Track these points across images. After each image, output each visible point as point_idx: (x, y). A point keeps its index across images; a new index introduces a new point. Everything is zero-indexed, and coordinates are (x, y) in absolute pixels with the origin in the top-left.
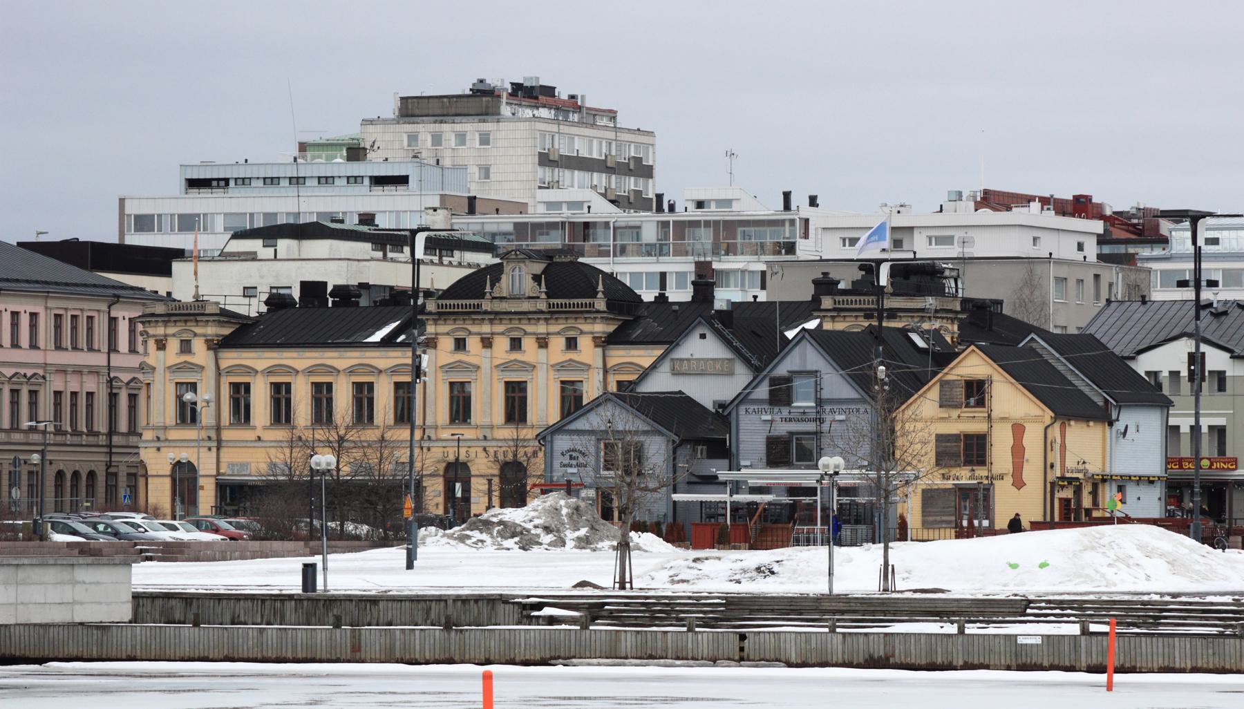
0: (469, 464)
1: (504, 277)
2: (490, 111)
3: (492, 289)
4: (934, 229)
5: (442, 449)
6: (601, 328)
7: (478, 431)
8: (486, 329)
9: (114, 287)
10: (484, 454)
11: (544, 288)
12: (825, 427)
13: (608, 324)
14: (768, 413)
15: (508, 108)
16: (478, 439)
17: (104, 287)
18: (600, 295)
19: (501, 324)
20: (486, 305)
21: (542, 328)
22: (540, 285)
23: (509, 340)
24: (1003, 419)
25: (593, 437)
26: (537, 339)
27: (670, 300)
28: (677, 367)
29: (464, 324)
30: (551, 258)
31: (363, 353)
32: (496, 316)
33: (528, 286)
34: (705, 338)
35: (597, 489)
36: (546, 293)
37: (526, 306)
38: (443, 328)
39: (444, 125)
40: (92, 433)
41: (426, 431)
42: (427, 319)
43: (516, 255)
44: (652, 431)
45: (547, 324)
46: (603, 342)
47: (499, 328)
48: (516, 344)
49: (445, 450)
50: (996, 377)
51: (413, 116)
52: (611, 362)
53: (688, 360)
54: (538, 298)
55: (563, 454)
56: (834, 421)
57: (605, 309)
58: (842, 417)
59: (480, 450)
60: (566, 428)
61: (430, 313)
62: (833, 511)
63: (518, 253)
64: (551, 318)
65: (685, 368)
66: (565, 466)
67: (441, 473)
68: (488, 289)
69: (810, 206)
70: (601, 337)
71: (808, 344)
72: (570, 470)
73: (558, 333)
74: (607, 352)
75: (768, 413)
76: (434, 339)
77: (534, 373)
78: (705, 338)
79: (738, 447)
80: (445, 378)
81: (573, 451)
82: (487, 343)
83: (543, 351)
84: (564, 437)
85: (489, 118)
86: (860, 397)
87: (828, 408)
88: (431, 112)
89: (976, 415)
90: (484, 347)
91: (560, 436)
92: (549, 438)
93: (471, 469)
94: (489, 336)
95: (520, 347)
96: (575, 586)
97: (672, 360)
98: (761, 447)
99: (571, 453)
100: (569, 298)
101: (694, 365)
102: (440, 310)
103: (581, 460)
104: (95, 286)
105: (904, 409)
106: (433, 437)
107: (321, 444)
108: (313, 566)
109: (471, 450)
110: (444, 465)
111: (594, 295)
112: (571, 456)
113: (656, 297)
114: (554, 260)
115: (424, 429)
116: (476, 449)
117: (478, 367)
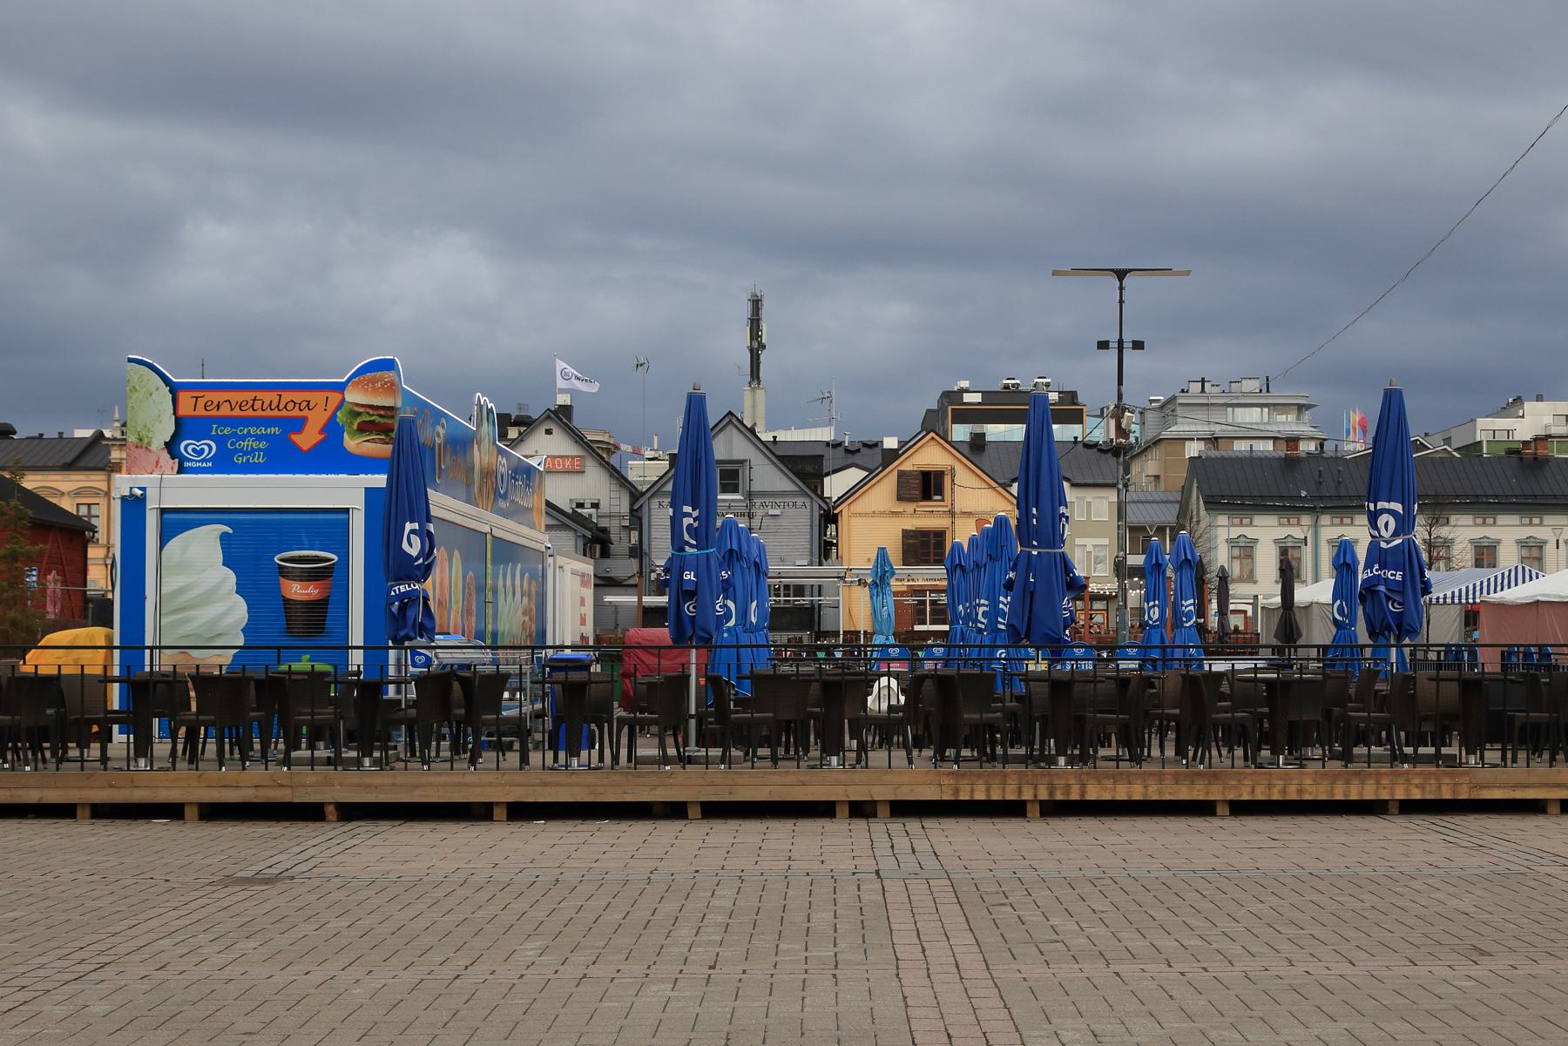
4: (112, 525)
12: (756, 523)
14: (770, 507)
24: (969, 514)
40: (1460, 603)
50: (959, 468)
56: (767, 515)
58: (777, 512)
62: (1256, 670)
69: (1098, 342)
71: (735, 431)
75: (770, 507)
78: (551, 433)
79: (649, 545)
86: (797, 489)
87: (758, 501)
89: (935, 509)
96: (114, 554)
98: (1469, 557)
105: (850, 503)
107: (631, 582)
115: (109, 548)
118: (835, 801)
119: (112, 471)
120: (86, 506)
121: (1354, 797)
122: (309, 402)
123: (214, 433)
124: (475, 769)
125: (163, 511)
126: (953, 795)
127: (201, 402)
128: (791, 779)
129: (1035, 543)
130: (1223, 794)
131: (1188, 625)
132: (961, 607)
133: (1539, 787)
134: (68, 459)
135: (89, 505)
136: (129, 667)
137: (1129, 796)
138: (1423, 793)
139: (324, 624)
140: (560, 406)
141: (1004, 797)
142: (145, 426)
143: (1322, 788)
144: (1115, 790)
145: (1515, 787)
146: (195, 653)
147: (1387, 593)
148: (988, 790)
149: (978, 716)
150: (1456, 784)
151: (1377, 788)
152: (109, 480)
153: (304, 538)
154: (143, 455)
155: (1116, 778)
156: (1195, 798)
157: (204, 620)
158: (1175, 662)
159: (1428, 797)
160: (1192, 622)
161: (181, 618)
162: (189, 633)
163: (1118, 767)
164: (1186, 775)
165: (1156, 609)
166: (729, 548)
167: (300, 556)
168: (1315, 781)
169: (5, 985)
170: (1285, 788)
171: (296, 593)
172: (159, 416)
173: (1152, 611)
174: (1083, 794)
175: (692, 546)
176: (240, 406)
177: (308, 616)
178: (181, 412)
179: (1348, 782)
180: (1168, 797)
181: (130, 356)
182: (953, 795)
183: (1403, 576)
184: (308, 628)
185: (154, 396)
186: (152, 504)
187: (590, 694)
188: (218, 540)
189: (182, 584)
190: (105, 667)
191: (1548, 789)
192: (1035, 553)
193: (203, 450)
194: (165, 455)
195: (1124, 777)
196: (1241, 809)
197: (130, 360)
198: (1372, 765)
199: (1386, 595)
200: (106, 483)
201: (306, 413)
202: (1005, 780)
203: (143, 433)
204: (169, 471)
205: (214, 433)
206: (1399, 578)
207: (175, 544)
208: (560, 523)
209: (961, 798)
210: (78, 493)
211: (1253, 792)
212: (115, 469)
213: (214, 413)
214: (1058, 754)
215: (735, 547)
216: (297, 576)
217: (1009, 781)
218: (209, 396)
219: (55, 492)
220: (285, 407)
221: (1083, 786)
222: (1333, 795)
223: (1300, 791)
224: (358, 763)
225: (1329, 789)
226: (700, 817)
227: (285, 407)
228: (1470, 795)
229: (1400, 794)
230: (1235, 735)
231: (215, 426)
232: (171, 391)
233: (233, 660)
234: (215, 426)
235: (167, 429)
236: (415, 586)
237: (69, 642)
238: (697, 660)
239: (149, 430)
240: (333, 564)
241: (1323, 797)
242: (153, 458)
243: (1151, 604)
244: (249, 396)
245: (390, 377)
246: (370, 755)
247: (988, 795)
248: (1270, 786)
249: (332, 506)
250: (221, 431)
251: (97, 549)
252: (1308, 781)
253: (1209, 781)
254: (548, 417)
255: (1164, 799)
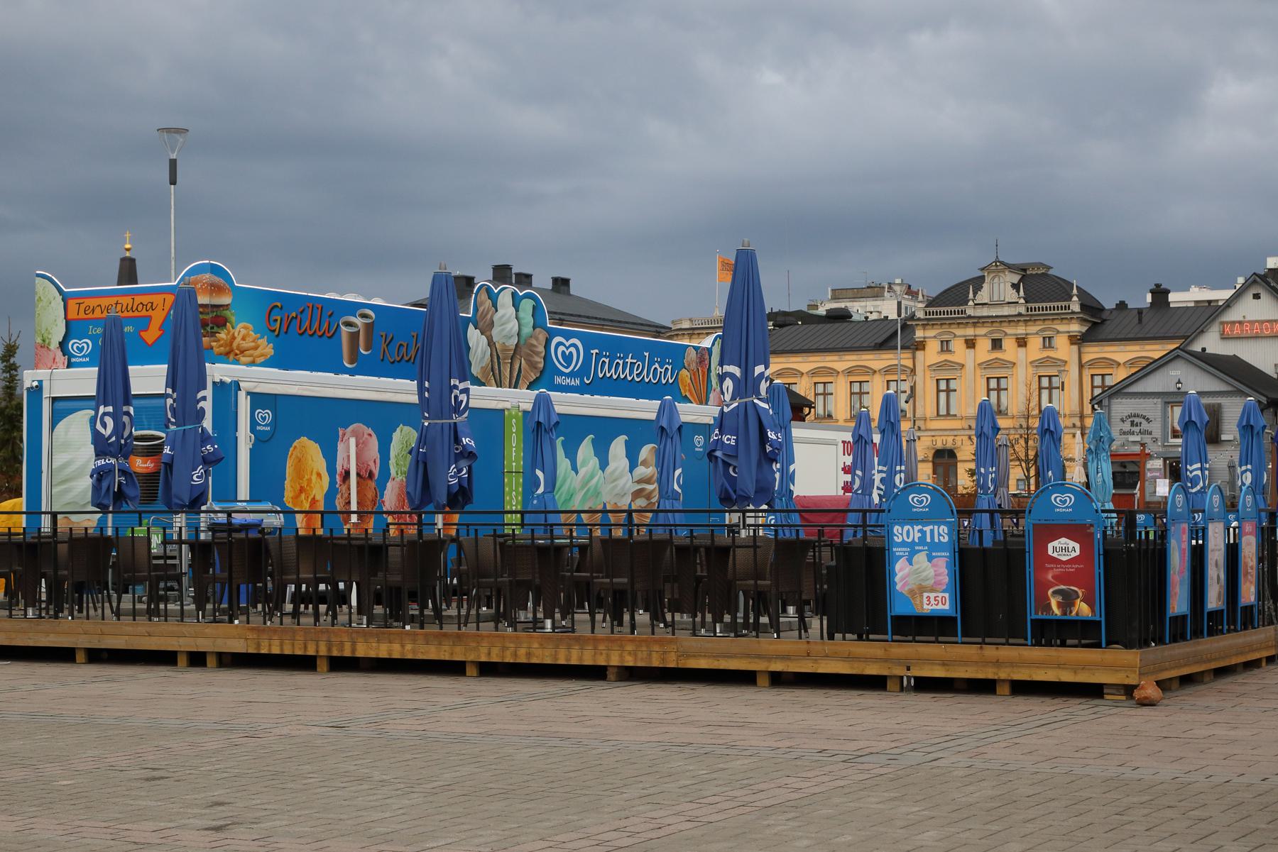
0: (955, 451)
1: (985, 286)
2: (880, 295)
3: (974, 297)
5: (930, 438)
6: (1076, 328)
7: (963, 421)
8: (970, 332)
9: (657, 327)
10: (970, 442)
11: (1022, 293)
13: (1082, 325)
15: (888, 294)
16: (963, 429)
17: (649, 326)
18: (1075, 298)
19: (983, 327)
20: (970, 312)
21: (1021, 330)
22: (1018, 291)
23: (990, 341)
25: (1159, 400)
26: (1017, 339)
27: (1129, 307)
28: (1227, 329)
29: (950, 328)
30: (1025, 270)
31: (859, 356)
32: (977, 321)
33: (1011, 295)
34: (1259, 298)
35: (1165, 460)
36: (1024, 299)
37: (1006, 311)
38: (931, 333)
39: (855, 303)
41: (916, 422)
42: (917, 325)
43: (996, 266)
44: (1235, 391)
45: (1026, 326)
46: (1079, 340)
47: (981, 331)
48: (997, 344)
49: (934, 439)
51: (839, 299)
52: (1086, 358)
53: (1240, 322)
54: (1017, 303)
55: (1123, 421)
57: (1079, 310)
59: (966, 438)
60: (1126, 391)
61: (919, 319)
63: (998, 264)
64: (1030, 320)
65: (1237, 331)
66: (1124, 433)
67: (931, 459)
68: (971, 296)
70: (1077, 336)
72: (1132, 438)
73: (1037, 333)
74: (1082, 349)
76: (923, 342)
77: (1014, 369)
78: (1259, 298)
80: (933, 376)
81: (1135, 416)
82: (970, 344)
83: (1022, 350)
84: (1124, 400)
85: (879, 298)
88: (848, 297)
90: (968, 347)
91: (1119, 400)
92: (1105, 402)
93: (958, 455)
94: (973, 338)
95: (1001, 347)
97: (1223, 323)
99: (1132, 419)
100: (1051, 301)
101: (1247, 327)
102: (928, 317)
103: (1145, 426)
104: (642, 325)
106: (923, 428)
108: (1035, 614)
109: (957, 438)
110: (933, 451)
111: (1070, 298)
112: (1132, 423)
113: (1117, 305)
114: (1028, 272)
115: (914, 421)
116: (962, 437)
117: (963, 366)
118: (755, 671)
119: (917, 349)
120: (1047, 378)
121: (574, 661)
122: (152, 303)
123: (90, 333)
124: (73, 619)
125: (54, 399)
126: (255, 649)
127: (82, 307)
128: (141, 629)
129: (426, 415)
130: (465, 655)
131: (1194, 490)
132: (1050, 473)
133: (741, 658)
134: (880, 340)
135: (1103, 376)
136: (117, 528)
137: (389, 654)
138: (635, 660)
139: (141, 493)
140: (1270, 270)
141: (293, 652)
142: (47, 330)
143: (547, 652)
144: (378, 648)
145: (716, 657)
146: (74, 518)
147: (726, 459)
148: (281, 645)
149: (614, 580)
150: (665, 652)
151: (595, 654)
152: (914, 358)
153: (144, 420)
154: (46, 353)
155: (459, 638)
156: (442, 658)
157: (79, 490)
158: (859, 528)
159: (639, 664)
160: (1198, 487)
161: (65, 488)
162: (69, 501)
163: (478, 629)
164: (436, 636)
165: (1249, 474)
166: (536, 420)
167: (141, 435)
168: (541, 645)
169: (631, 834)
170: (516, 652)
171: (139, 467)
172: (55, 320)
173: (1244, 476)
174: (354, 650)
175: (173, 424)
176: (108, 310)
177: (147, 486)
178: (70, 317)
179: (569, 648)
180: (420, 657)
181: (38, 272)
182: (255, 649)
183: (737, 441)
184: (148, 497)
185: (52, 304)
186: (46, 394)
187: (591, 556)
188: (88, 423)
189: (65, 460)
190: (102, 528)
191: (750, 660)
192: (426, 424)
193: (83, 347)
194: (59, 353)
195: (386, 636)
196: (489, 670)
197: (38, 275)
198: (121, 618)
199: (723, 461)
200: (912, 360)
201: (150, 312)
202: (294, 637)
203: (45, 335)
204: (61, 366)
205: (90, 333)
206: (733, 442)
207: (61, 426)
208: (1235, 389)
209: (263, 652)
210: (813, 373)
211: (489, 654)
212: (919, 347)
213: (90, 316)
214: (546, 617)
215: (541, 420)
216: (140, 453)
217: (297, 638)
218: (88, 302)
219: (1111, 362)
220: (137, 309)
221: (354, 644)
222: (556, 659)
223: (529, 655)
224: (536, 624)
225: (553, 653)
226: (84, 661)
227: (137, 309)
228: (678, 663)
229: (615, 661)
230: (587, 595)
231: (91, 327)
232: (63, 300)
233: (98, 524)
234: (91, 327)
235: (58, 332)
236: (109, 460)
237: (10, 508)
238: (113, 523)
239: (49, 333)
240: (163, 442)
241: (548, 661)
242: (51, 357)
243: (1244, 468)
244: (113, 300)
245: (207, 278)
246: (721, 621)
247: (282, 649)
248: (504, 649)
249: (144, 393)
250: (95, 331)
251: (1007, 420)
252: (536, 645)
253: (453, 642)
254: (1255, 282)
255: (417, 658)
